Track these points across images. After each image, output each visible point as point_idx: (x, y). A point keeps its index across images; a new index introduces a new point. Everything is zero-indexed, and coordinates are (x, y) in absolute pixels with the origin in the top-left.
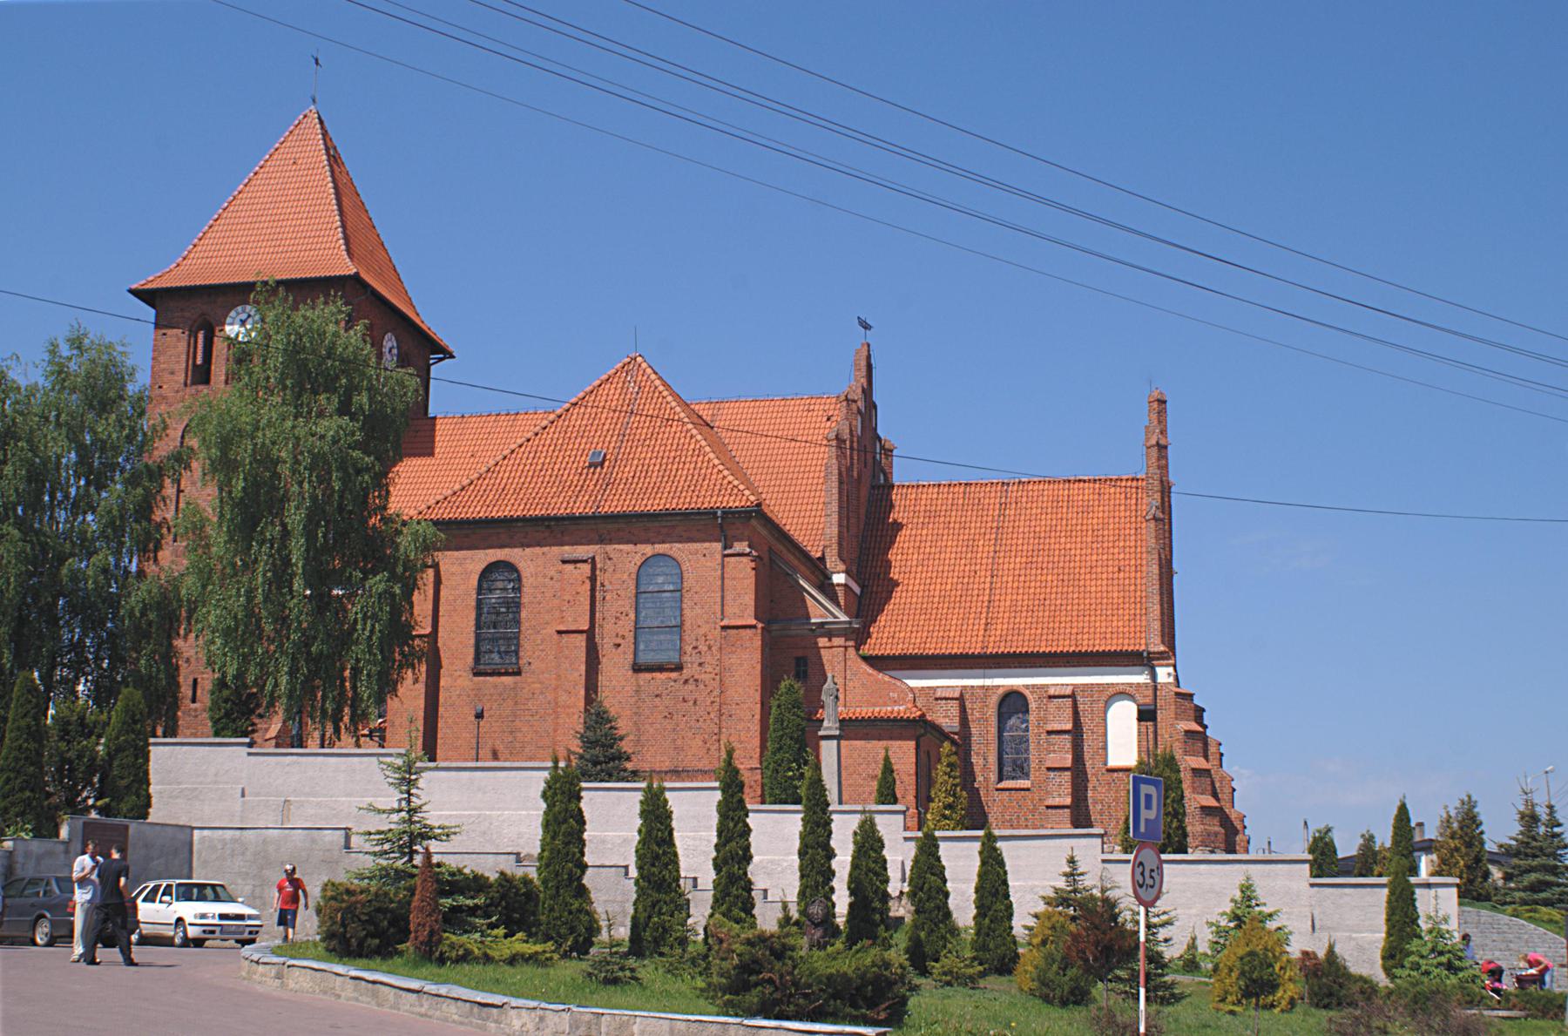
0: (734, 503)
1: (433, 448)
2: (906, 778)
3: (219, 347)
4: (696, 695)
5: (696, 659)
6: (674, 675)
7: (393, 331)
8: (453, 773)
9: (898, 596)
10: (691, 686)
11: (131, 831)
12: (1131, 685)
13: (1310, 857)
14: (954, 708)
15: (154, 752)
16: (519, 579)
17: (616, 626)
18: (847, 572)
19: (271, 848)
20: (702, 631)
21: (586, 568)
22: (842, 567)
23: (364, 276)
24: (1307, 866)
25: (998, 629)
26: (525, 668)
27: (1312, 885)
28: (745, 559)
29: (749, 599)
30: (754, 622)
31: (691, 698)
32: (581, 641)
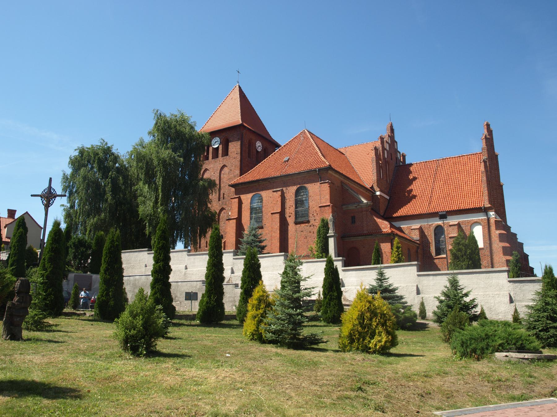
0: (322, 166)
1: (503, 249)
2: (388, 254)
3: (211, 149)
4: (314, 230)
5: (313, 218)
6: (307, 224)
7: (260, 141)
8: (201, 256)
9: (187, 115)
10: (312, 227)
11: (93, 277)
12: (479, 219)
13: (506, 268)
14: (417, 232)
15: (123, 255)
16: (262, 199)
17: (290, 210)
18: (380, 191)
19: (137, 282)
20: (315, 209)
21: (280, 193)
22: (379, 189)
23: (245, 124)
24: (506, 273)
25: (432, 205)
26: (264, 226)
27: (234, 259)
28: (326, 184)
29: (328, 197)
30: (329, 204)
31: (312, 231)
32: (278, 216)
